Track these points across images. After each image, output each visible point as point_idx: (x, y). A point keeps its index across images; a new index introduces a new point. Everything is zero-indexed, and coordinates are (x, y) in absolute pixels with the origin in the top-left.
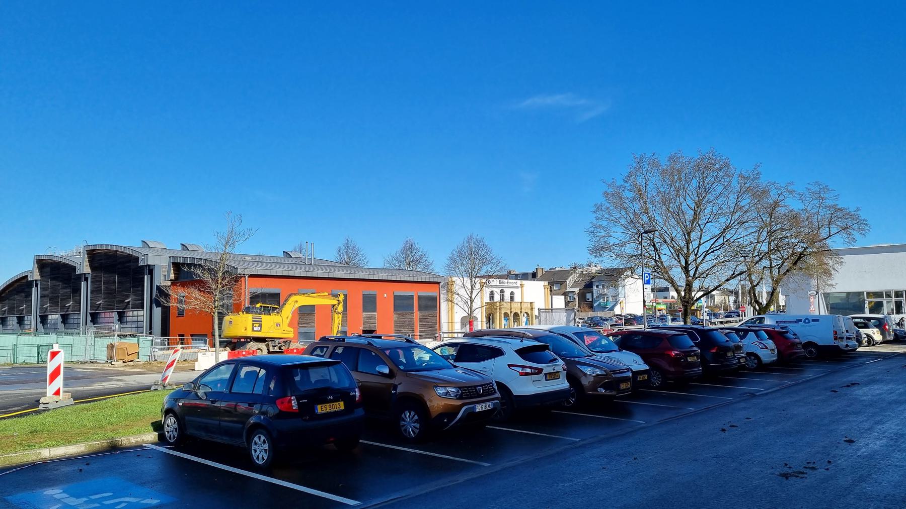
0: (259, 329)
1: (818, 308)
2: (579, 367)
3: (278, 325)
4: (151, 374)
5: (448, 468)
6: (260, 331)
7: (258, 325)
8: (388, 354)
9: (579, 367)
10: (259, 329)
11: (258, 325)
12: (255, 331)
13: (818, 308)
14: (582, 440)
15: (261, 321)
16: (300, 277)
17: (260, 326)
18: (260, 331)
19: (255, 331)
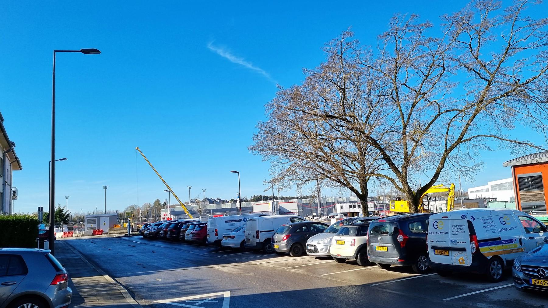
0: (393, 208)
1: (67, 274)
2: (6, 157)
3: (402, 206)
4: (136, 275)
5: (89, 297)
6: (394, 209)
7: (393, 206)
8: (532, 279)
9: (6, 157)
10: (393, 208)
11: (393, 206)
12: (392, 209)
13: (67, 274)
14: (211, 257)
15: (394, 204)
16: (522, 165)
17: (394, 206)
18: (394, 209)
19: (392, 209)
